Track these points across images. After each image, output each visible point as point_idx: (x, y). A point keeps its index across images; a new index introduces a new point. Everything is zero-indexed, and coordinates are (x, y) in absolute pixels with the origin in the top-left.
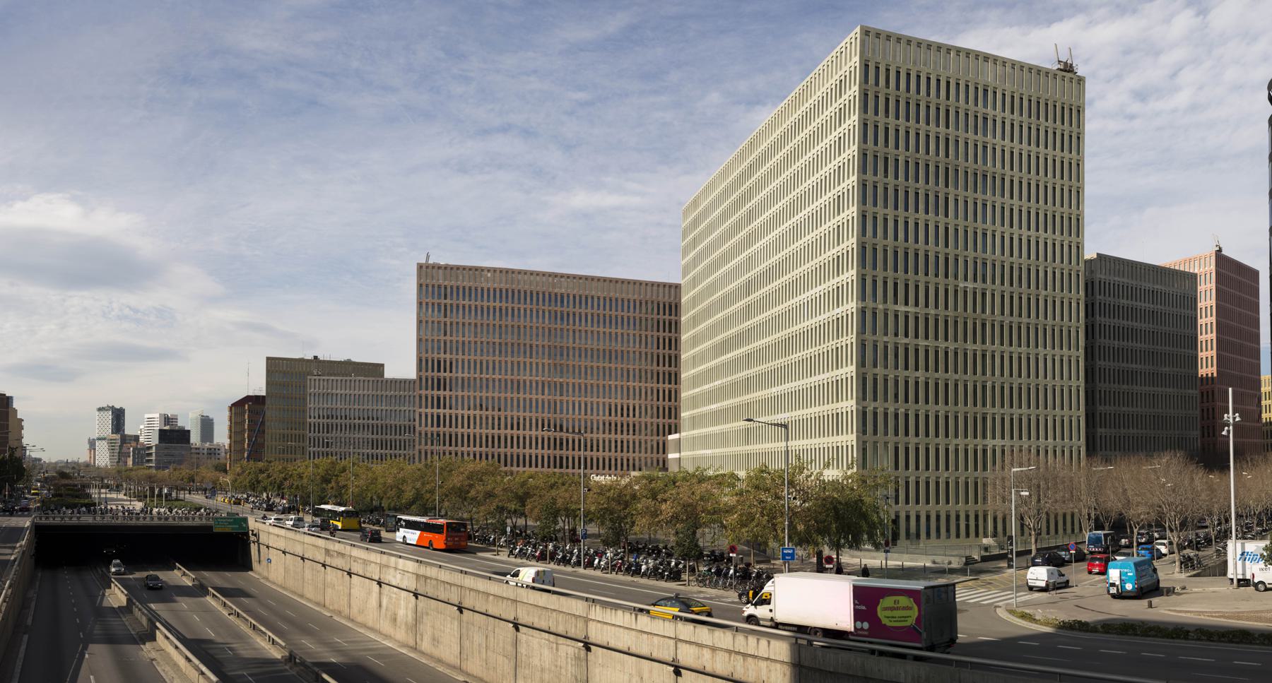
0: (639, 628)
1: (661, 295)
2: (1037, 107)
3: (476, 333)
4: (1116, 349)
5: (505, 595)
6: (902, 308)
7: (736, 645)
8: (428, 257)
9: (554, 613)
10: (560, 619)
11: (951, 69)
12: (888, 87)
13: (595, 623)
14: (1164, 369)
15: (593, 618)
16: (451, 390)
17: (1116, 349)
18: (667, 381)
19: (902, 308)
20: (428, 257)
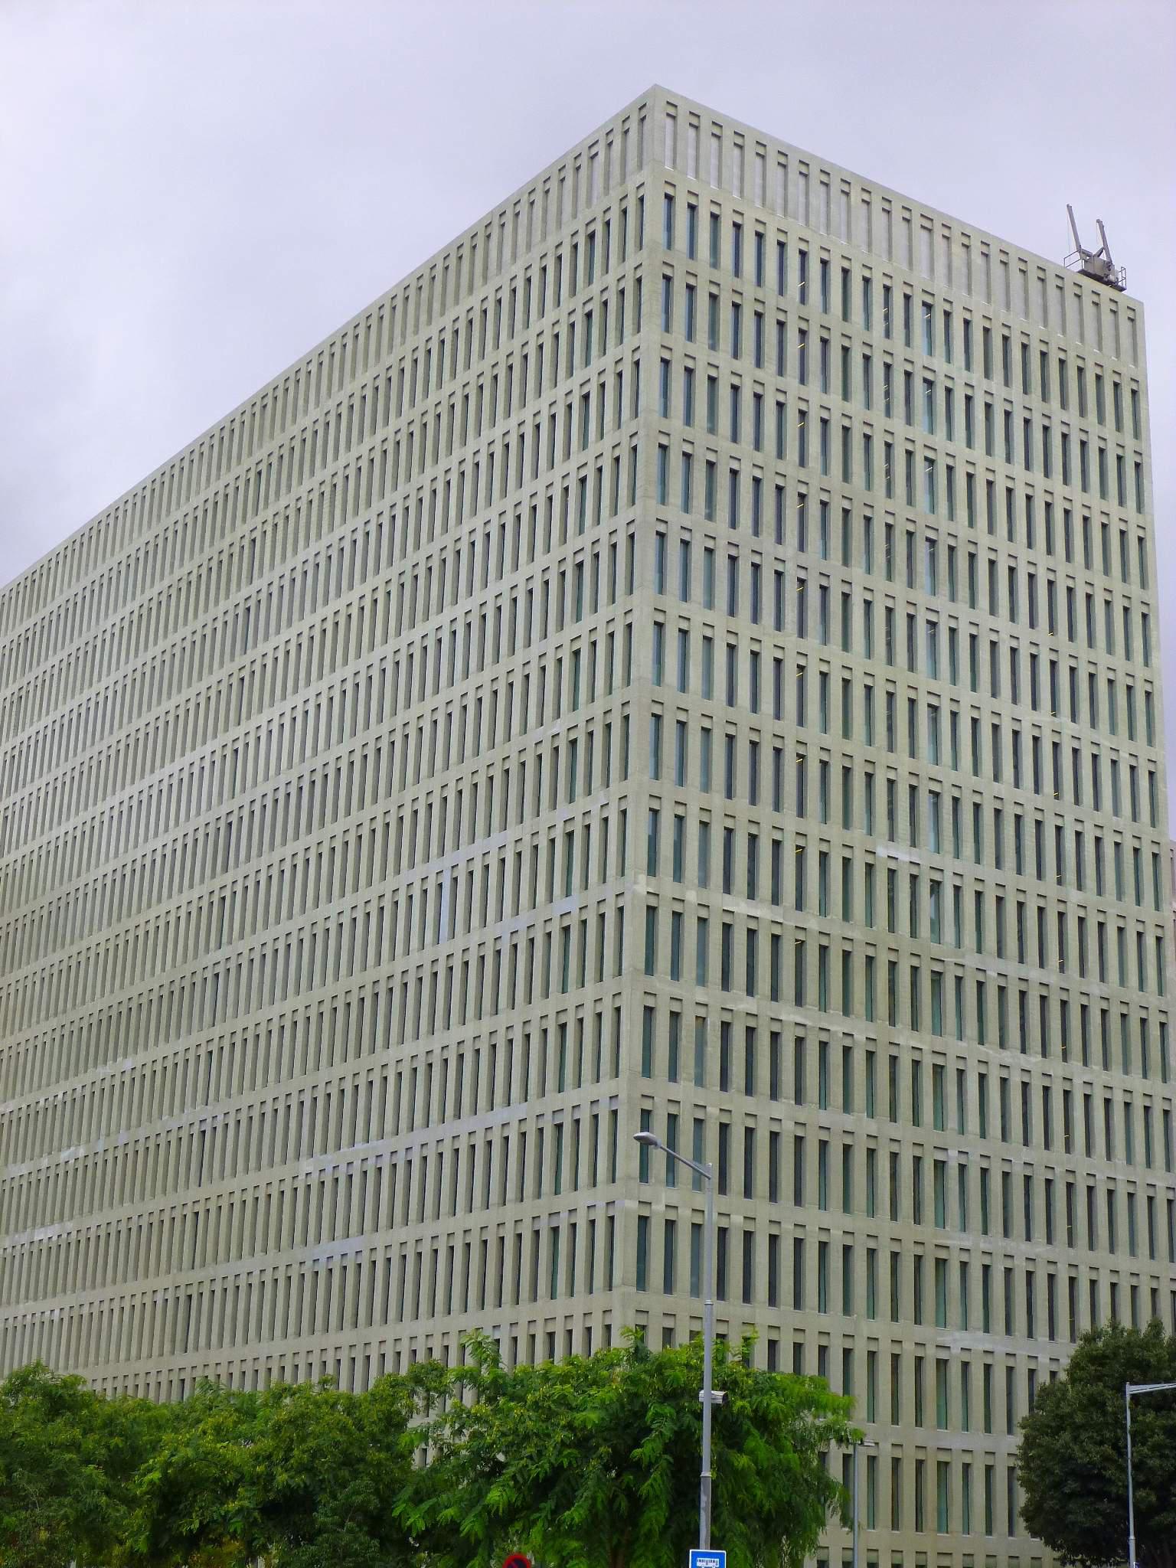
6: (741, 906)
19: (741, 906)
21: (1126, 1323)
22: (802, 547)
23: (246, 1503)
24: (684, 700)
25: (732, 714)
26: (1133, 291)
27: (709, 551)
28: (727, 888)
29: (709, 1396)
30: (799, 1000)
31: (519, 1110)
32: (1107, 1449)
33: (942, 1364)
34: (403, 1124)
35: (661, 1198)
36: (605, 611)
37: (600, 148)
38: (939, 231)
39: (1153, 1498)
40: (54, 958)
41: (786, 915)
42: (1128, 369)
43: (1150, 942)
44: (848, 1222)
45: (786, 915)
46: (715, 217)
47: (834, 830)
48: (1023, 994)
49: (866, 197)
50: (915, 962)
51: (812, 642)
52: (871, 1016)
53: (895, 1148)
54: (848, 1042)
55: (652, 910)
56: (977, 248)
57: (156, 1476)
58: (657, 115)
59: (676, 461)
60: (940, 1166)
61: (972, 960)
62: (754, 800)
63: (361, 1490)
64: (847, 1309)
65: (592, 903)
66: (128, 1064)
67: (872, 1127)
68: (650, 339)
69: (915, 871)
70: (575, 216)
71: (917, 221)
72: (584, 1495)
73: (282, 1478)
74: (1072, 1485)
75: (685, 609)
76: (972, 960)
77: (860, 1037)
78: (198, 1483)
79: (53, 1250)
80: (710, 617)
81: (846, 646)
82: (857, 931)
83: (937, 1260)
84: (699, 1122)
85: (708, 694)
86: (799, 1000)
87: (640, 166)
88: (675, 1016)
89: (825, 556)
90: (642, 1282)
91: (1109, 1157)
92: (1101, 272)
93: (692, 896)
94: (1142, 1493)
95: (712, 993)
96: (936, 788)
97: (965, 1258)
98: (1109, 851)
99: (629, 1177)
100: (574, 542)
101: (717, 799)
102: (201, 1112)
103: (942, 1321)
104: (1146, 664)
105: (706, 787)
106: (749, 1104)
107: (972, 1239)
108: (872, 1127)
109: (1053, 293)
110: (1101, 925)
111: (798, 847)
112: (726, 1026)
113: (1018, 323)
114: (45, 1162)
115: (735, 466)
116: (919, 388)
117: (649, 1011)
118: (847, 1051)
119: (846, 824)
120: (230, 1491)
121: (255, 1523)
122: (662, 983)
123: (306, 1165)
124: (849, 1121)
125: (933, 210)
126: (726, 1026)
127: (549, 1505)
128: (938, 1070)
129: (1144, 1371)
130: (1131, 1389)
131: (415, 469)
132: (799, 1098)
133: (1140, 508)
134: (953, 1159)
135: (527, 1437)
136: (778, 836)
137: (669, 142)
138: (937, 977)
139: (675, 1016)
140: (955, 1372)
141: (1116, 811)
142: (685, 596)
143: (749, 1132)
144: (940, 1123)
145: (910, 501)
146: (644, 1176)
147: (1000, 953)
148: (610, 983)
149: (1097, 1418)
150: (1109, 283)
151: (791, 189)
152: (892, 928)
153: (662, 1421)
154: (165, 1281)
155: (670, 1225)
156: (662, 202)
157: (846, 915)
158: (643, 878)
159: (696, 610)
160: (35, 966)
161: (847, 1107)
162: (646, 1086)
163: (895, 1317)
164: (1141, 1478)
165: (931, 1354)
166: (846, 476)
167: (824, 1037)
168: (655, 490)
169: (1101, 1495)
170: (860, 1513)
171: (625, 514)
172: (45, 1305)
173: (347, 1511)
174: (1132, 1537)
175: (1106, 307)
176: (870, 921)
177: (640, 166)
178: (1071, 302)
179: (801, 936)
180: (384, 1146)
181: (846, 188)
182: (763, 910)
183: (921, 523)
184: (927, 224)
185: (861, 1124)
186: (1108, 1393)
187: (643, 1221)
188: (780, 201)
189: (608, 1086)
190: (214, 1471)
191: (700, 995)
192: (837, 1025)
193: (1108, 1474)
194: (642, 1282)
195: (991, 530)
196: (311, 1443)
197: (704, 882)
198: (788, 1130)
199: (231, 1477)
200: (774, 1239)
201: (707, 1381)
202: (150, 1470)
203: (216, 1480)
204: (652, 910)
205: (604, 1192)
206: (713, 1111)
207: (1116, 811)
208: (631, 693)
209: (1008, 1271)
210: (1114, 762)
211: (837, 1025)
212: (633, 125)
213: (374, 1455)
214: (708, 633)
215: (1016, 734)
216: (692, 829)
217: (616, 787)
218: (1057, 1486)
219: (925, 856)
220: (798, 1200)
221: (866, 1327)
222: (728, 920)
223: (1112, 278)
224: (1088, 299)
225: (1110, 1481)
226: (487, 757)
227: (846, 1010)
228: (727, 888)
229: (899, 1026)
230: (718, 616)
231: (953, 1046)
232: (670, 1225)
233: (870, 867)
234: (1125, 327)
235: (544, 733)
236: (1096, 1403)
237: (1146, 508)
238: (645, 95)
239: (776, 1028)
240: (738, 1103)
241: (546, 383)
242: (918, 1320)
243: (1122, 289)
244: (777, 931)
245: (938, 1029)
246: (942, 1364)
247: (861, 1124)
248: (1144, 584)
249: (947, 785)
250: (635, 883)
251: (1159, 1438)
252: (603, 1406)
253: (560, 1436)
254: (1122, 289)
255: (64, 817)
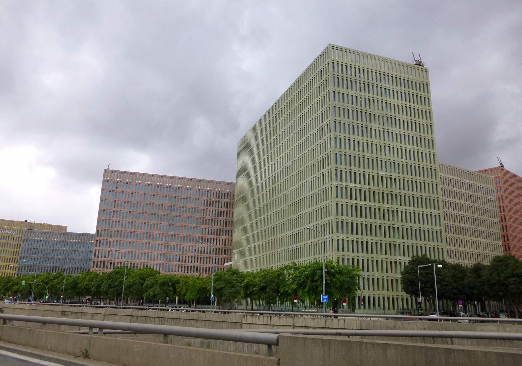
0: (272, 324)
1: (182, 203)
2: (409, 83)
3: (131, 207)
4: (453, 215)
5: (191, 318)
6: (353, 185)
7: (326, 325)
8: (109, 167)
9: (222, 323)
10: (225, 326)
11: (368, 65)
12: (343, 73)
13: (246, 325)
14: (481, 228)
15: (245, 322)
16: (99, 247)
17: (453, 215)
18: (224, 235)
19: (353, 185)
20: (109, 167)
21: (420, 254)
22: (362, 121)
23: (257, 288)
24: (341, 150)
25: (350, 151)
26: (426, 66)
27: (344, 124)
28: (351, 182)
29: (325, 270)
30: (365, 200)
31: (318, 222)
32: (415, 277)
33: (396, 263)
34: (302, 225)
35: (341, 236)
36: (327, 136)
37: (322, 56)
38: (386, 61)
39: (423, 286)
40: (251, 200)
41: (362, 186)
42: (426, 81)
43: (434, 185)
44: (376, 238)
45: (362, 186)
46: (342, 65)
47: (371, 170)
48: (409, 196)
49: (371, 57)
50: (387, 192)
51: (365, 137)
52: (379, 202)
53: (385, 225)
54: (375, 207)
55: (337, 187)
56: (393, 63)
57: (244, 284)
58: (330, 49)
59: (337, 109)
60: (394, 228)
61: (398, 191)
62: (355, 166)
63: (273, 286)
64: (377, 253)
65: (327, 186)
66: (262, 217)
67: (380, 221)
68: (331, 88)
69: (386, 176)
70: (319, 68)
71: (381, 60)
72: (308, 286)
73: (262, 284)
74: (409, 283)
75: (340, 134)
76: (398, 191)
77: (377, 206)
78: (251, 285)
79: (254, 248)
80: (345, 135)
81: (371, 137)
82: (376, 188)
83: (394, 244)
84: (347, 223)
85: (345, 148)
86: (365, 200)
87: (328, 58)
88: (342, 205)
89: (366, 122)
90: (338, 250)
91: (428, 224)
92: (419, 64)
93: (344, 184)
94: (421, 285)
95: (349, 200)
96: (390, 161)
97: (399, 243)
98: (425, 169)
99: (335, 233)
100: (322, 124)
101: (348, 167)
102: (273, 224)
103: (395, 255)
104: (432, 134)
105: (346, 165)
106: (357, 219)
107: (401, 240)
108: (380, 221)
109: (409, 69)
110: (424, 183)
111: (364, 174)
112: (351, 206)
113: (402, 75)
114: (252, 234)
115: (348, 108)
116: (383, 89)
117: (337, 204)
118: (375, 209)
119: (373, 169)
120: (255, 286)
121: (258, 291)
122: (339, 199)
123: (288, 233)
124: (375, 221)
125: (384, 57)
126: (351, 206)
127: (302, 288)
128: (393, 211)
129: (422, 263)
130: (419, 266)
131: (298, 114)
132: (366, 217)
133: (429, 106)
134: (396, 226)
135: (298, 277)
136: (360, 172)
137: (333, 53)
138: (392, 195)
139: (342, 205)
140: (398, 264)
141: (427, 162)
142: (340, 132)
143: (357, 224)
144: (393, 220)
145: (382, 110)
146: (338, 232)
147: (404, 189)
148: (330, 200)
149: (413, 271)
150: (421, 65)
151: (356, 58)
152: (382, 186)
153: (318, 273)
154: (269, 252)
155: (343, 240)
156: (332, 64)
157: (374, 185)
158: (335, 182)
159: (342, 134)
160: (249, 201)
161: (375, 218)
162: (337, 217)
163: (386, 254)
164: (421, 282)
165: (393, 261)
166: (370, 107)
167: (370, 207)
168: (333, 114)
169: (415, 285)
170: (362, 287)
171: (329, 119)
172: (253, 257)
173: (271, 289)
174: (420, 292)
175: (420, 70)
176: (378, 186)
177: (328, 58)
178: (413, 70)
179: (365, 189)
180: (299, 229)
181: (367, 56)
182: (358, 185)
183: (385, 114)
184: (383, 60)
185: (378, 221)
186: (415, 267)
187: (338, 240)
188: (354, 60)
189: (331, 218)
190: (253, 283)
191: (346, 201)
192: (373, 204)
193: (415, 281)
194: (338, 250)
195: (399, 114)
196: (266, 279)
197: (346, 181)
198: (364, 223)
199: (255, 284)
200: (362, 242)
201: (324, 267)
202: (243, 283)
203: (253, 285)
204: (337, 187)
205: (331, 235)
206: (350, 220)
207: (427, 162)
208: (331, 150)
209: (408, 246)
210: (426, 153)
211: (373, 204)
212: (327, 51)
213: (277, 280)
214: (345, 138)
215: (406, 150)
216: (344, 173)
217: (330, 166)
218: (407, 283)
219: (388, 173)
220: (367, 235)
221: (381, 256)
222: (351, 187)
223: (421, 64)
224: (416, 69)
225: (416, 283)
226: (308, 164)
227: (374, 201)
228: (351, 182)
229: (385, 204)
230: (347, 135)
231: (395, 207)
232: (343, 240)
233: (378, 176)
234: (425, 73)
235: (319, 158)
236: (413, 269)
237: (430, 106)
238: (328, 46)
239: (361, 205)
240: (354, 219)
241: (316, 98)
242: (391, 255)
243: (423, 66)
244: (360, 189)
245: (392, 204)
246: (396, 263)
247: (378, 221)
248: (431, 120)
249: (392, 160)
250: (333, 182)
251: (424, 275)
252: (309, 271)
253: (303, 276)
254: (423, 66)
255: (294, 171)
